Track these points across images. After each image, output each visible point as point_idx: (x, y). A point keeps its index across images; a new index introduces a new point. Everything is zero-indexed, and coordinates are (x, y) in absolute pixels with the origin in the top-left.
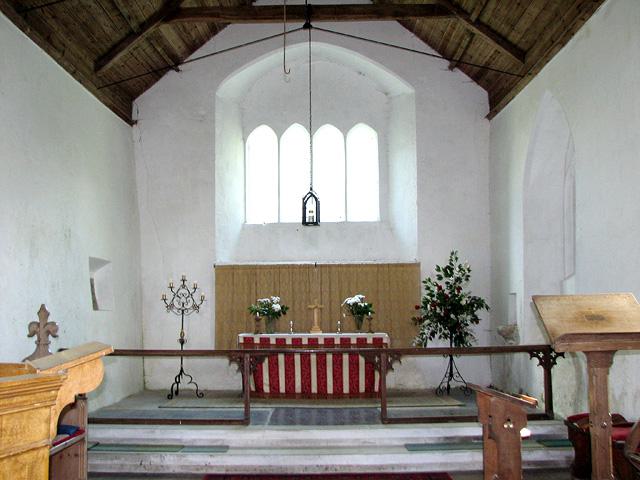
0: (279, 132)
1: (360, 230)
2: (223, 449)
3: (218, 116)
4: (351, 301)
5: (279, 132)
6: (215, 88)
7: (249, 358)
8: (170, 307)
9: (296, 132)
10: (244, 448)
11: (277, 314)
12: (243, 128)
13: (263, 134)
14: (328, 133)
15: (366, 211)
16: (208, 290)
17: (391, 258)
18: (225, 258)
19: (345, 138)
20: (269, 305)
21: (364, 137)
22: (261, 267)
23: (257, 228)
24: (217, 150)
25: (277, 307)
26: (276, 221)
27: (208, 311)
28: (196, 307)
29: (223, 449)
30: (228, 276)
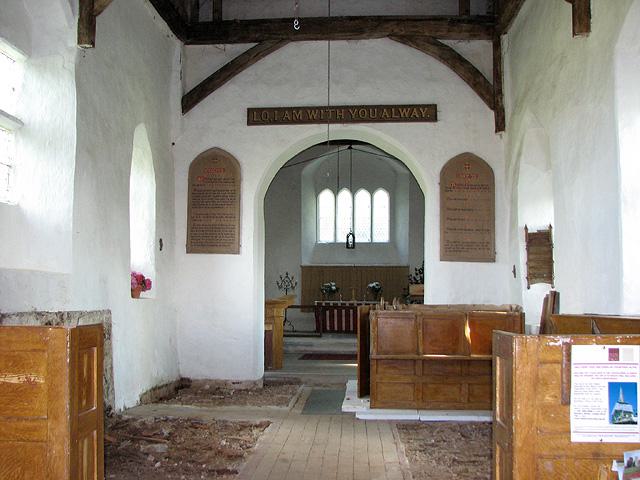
0: (336, 193)
1: (371, 246)
2: (311, 345)
3: (303, 185)
4: (371, 285)
5: (336, 193)
6: (301, 170)
7: (320, 312)
8: (280, 287)
9: (345, 194)
10: (321, 345)
11: (334, 292)
12: (316, 191)
13: (326, 196)
14: (363, 195)
15: (382, 236)
16: (298, 279)
17: (394, 264)
18: (306, 262)
19: (497, 46)
20: (330, 287)
21: (382, 197)
22: (326, 267)
23: (324, 245)
24: (303, 211)
25: (334, 288)
26: (331, 240)
27: (298, 291)
28: (293, 288)
29: (311, 345)
30: (307, 271)
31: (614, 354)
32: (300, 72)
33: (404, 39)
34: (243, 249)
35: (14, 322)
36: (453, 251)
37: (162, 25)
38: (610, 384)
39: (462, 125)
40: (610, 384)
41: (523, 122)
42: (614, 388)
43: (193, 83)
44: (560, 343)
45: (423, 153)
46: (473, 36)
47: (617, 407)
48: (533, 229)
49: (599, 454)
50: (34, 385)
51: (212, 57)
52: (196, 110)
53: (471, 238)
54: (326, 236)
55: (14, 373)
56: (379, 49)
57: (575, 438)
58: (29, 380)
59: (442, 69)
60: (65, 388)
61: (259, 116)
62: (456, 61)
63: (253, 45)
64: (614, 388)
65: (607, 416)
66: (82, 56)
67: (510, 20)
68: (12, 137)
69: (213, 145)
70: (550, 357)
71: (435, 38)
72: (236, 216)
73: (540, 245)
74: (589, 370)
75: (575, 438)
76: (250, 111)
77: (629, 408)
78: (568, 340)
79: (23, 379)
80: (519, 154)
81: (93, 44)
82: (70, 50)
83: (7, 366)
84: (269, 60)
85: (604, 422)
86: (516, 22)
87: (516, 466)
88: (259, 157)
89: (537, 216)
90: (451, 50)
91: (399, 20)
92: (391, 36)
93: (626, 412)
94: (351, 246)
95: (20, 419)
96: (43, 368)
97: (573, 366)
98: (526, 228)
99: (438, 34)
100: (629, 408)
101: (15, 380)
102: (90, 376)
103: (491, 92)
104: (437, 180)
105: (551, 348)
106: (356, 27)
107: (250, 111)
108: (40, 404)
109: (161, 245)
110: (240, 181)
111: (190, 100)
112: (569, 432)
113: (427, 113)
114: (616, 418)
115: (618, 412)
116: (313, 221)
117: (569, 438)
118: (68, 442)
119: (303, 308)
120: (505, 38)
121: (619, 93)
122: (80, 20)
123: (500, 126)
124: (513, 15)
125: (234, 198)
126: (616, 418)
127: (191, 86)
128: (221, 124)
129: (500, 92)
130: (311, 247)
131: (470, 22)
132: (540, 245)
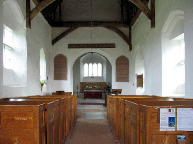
1: (97, 77)
13: (86, 65)
14: (95, 64)
18: (81, 81)
19: (130, 29)
21: (100, 65)
24: (81, 68)
26: (88, 76)
31: (170, 111)
32: (82, 35)
33: (108, 27)
34: (68, 79)
35: (11, 100)
36: (119, 79)
37: (46, 22)
38: (169, 117)
39: (121, 48)
40: (169, 117)
41: (137, 48)
42: (170, 118)
43: (54, 37)
44: (157, 108)
45: (112, 56)
46: (124, 26)
47: (170, 123)
48: (139, 74)
49: (166, 133)
50: (30, 120)
51: (60, 30)
52: (55, 44)
53: (123, 76)
54: (86, 75)
55: (24, 117)
56: (101, 29)
57: (161, 130)
58: (28, 119)
59: (116, 35)
60: (38, 121)
61: (71, 46)
62: (120, 33)
63: (70, 28)
64: (170, 118)
65: (168, 125)
66: (27, 31)
67: (133, 23)
68: (9, 52)
69: (60, 53)
70: (155, 111)
71: (115, 27)
72: (66, 71)
73: (140, 78)
74: (164, 114)
75: (161, 130)
76: (69, 45)
77: (173, 123)
78: (159, 107)
79: (27, 119)
80: (136, 56)
81: (30, 28)
82: (24, 29)
83: (22, 116)
84: (74, 32)
85: (167, 126)
86: (135, 23)
87: (147, 137)
88: (72, 56)
89: (141, 71)
90: (119, 30)
91: (107, 22)
92: (104, 26)
93: (172, 124)
94: (92, 77)
95: (26, 128)
96: (32, 116)
97: (160, 113)
98: (137, 74)
99: (116, 26)
100: (173, 123)
101: (24, 119)
102: (43, 117)
103: (128, 40)
104: (115, 62)
105: (155, 109)
106: (97, 23)
107: (69, 45)
108: (32, 125)
109: (48, 78)
110: (67, 62)
111: (54, 41)
112: (159, 128)
113: (112, 46)
114: (170, 125)
115: (170, 124)
116: (83, 71)
117: (159, 130)
118: (39, 133)
119: (81, 92)
120: (132, 27)
121: (162, 43)
122: (27, 21)
123: (131, 49)
124: (135, 21)
125: (65, 67)
126: (170, 125)
127: (54, 38)
128: (62, 47)
129: (131, 41)
130: (83, 77)
131: (124, 23)
132: (140, 78)
